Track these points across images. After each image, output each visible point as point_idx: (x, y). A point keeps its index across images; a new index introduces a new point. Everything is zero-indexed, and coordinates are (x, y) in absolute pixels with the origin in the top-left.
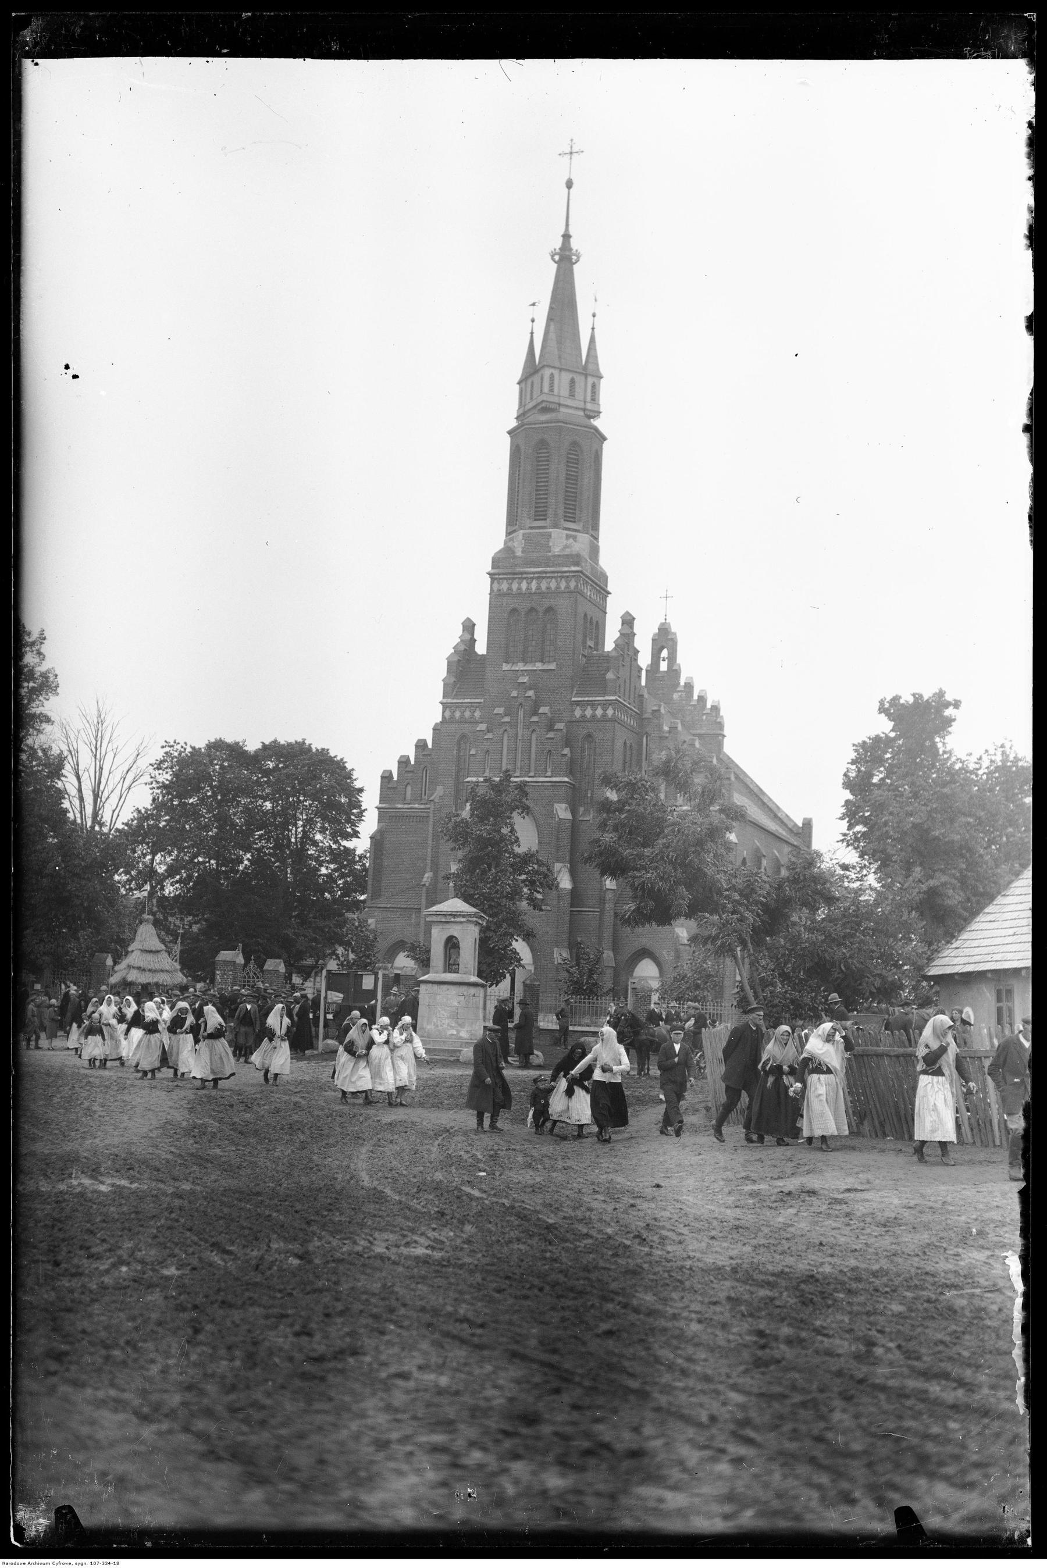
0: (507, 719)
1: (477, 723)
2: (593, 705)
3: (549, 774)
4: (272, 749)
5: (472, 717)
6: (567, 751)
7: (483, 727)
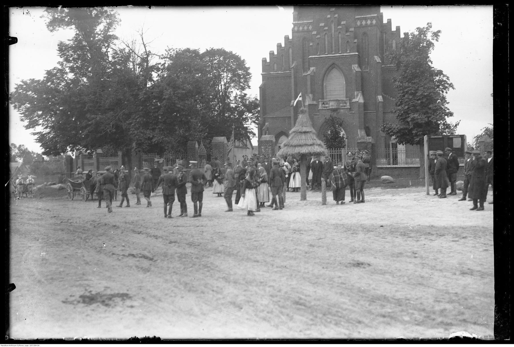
0: (326, 28)
1: (312, 31)
2: (366, 19)
3: (348, 52)
4: (211, 53)
5: (308, 29)
6: (356, 41)
7: (315, 33)
